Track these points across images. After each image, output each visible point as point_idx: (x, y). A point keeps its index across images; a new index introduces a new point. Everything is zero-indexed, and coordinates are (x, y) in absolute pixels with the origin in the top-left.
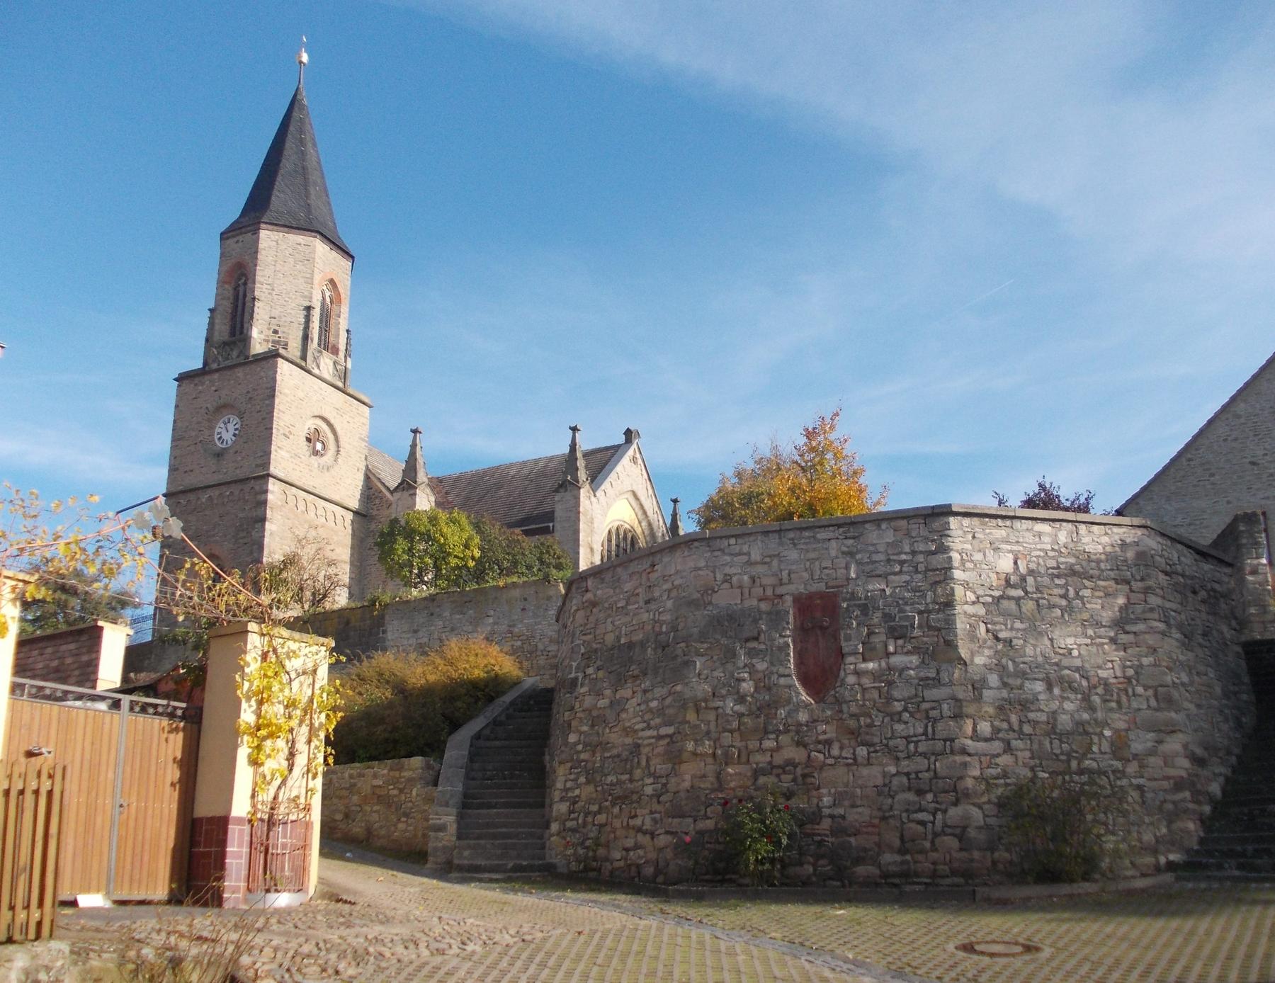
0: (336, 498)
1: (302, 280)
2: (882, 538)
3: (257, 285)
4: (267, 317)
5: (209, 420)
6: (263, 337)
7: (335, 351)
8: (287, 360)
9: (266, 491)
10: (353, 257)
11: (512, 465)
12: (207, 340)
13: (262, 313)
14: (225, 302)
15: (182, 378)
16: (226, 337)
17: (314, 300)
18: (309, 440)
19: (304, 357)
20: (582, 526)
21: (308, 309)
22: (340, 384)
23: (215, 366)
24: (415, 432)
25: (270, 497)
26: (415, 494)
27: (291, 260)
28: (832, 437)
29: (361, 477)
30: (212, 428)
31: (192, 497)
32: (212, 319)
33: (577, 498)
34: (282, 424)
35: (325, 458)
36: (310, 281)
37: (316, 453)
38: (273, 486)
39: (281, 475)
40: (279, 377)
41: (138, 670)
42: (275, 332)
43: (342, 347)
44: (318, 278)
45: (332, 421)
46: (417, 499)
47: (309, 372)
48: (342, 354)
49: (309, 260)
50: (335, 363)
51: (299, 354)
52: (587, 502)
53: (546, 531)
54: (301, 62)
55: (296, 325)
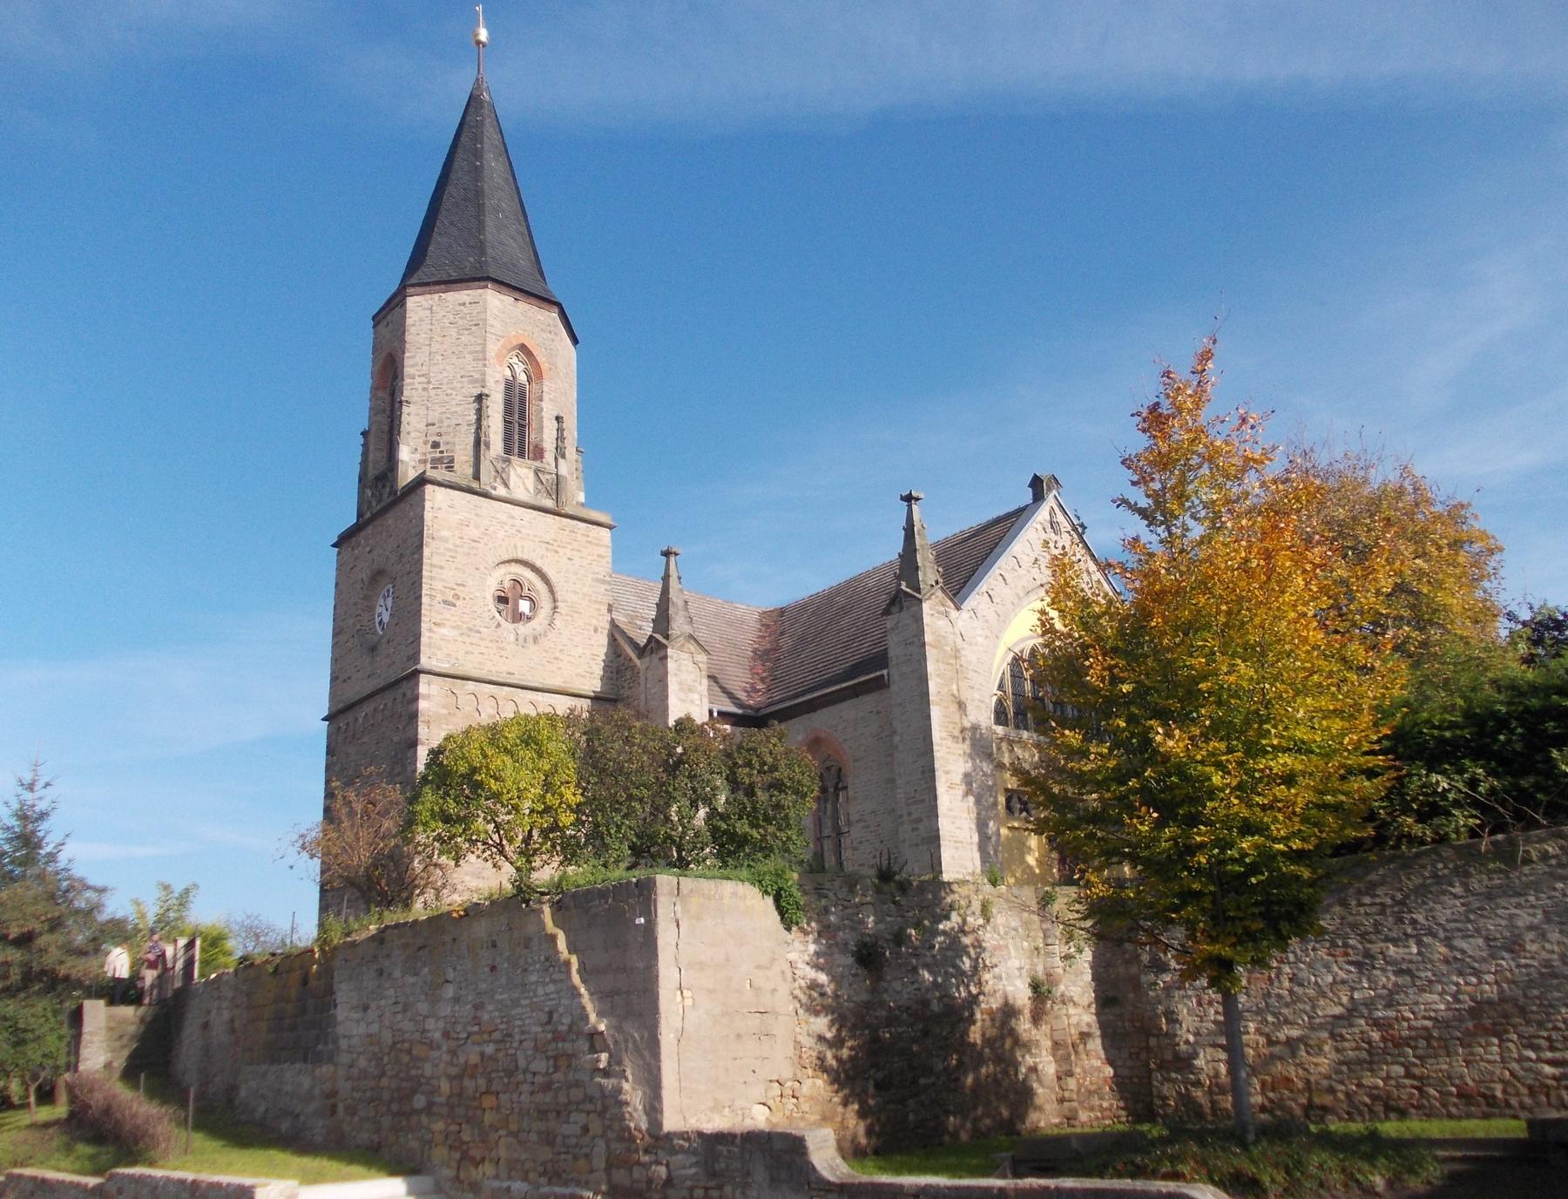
0: (556, 682)
1: (469, 357)
2: (481, 929)
3: (407, 381)
4: (422, 426)
5: (366, 598)
6: (418, 456)
7: (539, 453)
8: (440, 484)
9: (416, 698)
10: (559, 305)
11: (868, 575)
12: (360, 481)
13: (413, 420)
14: (379, 418)
15: (344, 540)
16: (382, 465)
17: (490, 383)
18: (502, 600)
19: (477, 477)
20: (931, 667)
21: (480, 398)
22: (549, 503)
23: (368, 515)
24: (667, 554)
25: (423, 705)
26: (666, 657)
27: (453, 332)
28: (1205, 415)
29: (603, 640)
30: (371, 609)
31: (350, 717)
32: (365, 446)
33: (919, 619)
34: (438, 585)
35: (533, 623)
36: (481, 357)
37: (518, 617)
38: (425, 686)
39: (444, 667)
40: (428, 515)
41: (558, 907)
42: (435, 445)
43: (549, 444)
44: (493, 348)
45: (538, 564)
46: (671, 665)
47: (486, 495)
48: (549, 456)
49: (479, 324)
50: (537, 472)
51: (470, 471)
52: (943, 622)
53: (880, 684)
54: (478, 42)
55: (464, 428)
